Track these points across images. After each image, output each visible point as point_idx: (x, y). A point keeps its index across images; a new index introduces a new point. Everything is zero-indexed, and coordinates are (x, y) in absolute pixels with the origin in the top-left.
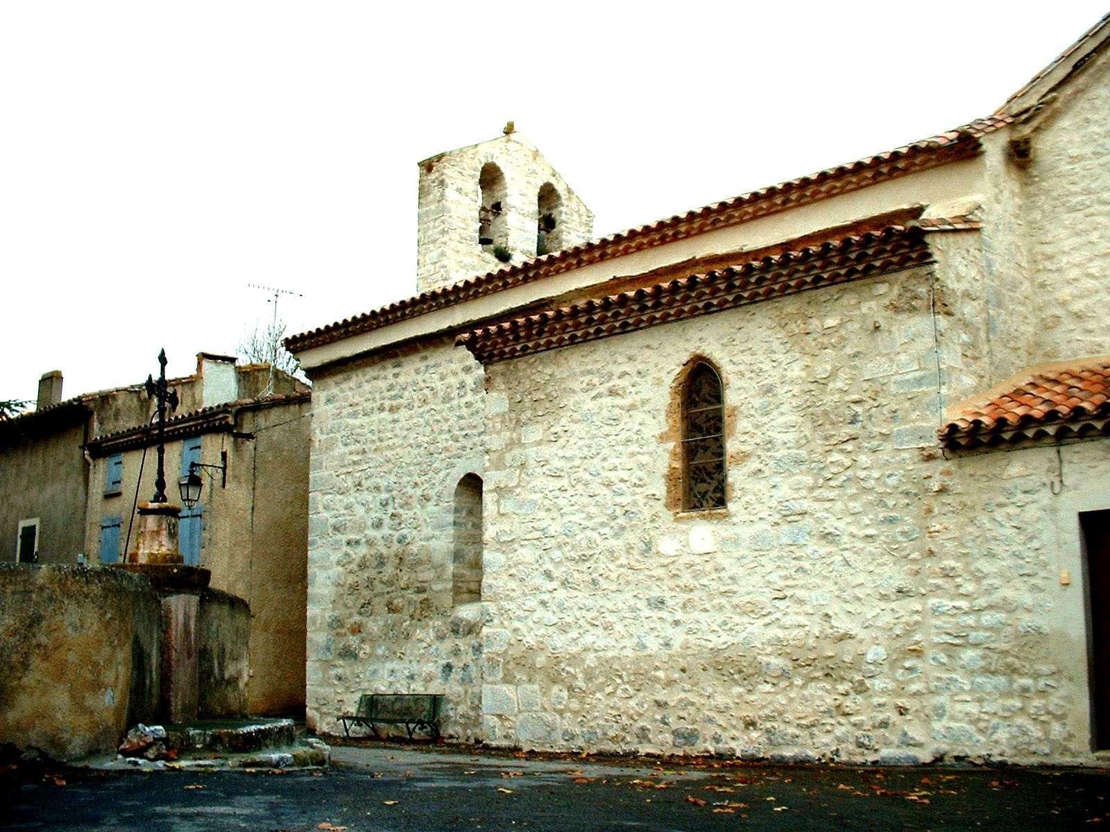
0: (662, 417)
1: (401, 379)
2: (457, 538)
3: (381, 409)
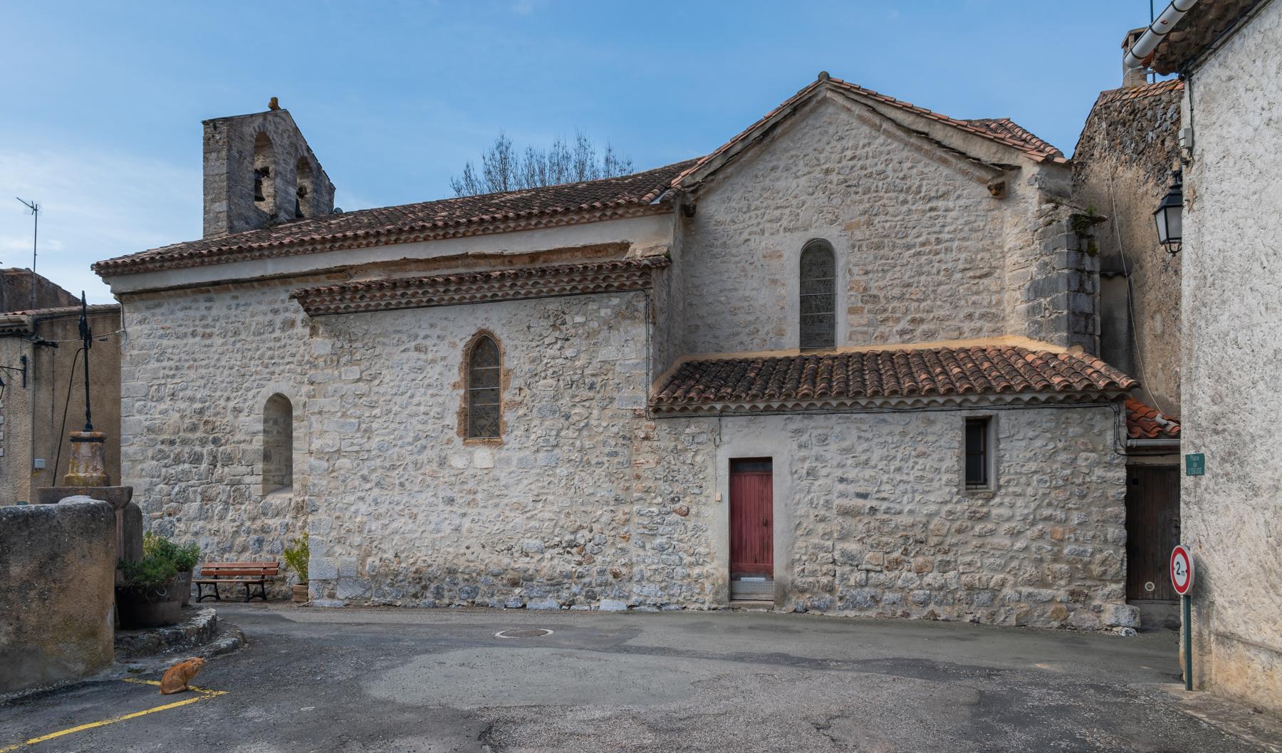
0: (456, 370)
1: (214, 312)
2: (266, 442)
3: (194, 334)
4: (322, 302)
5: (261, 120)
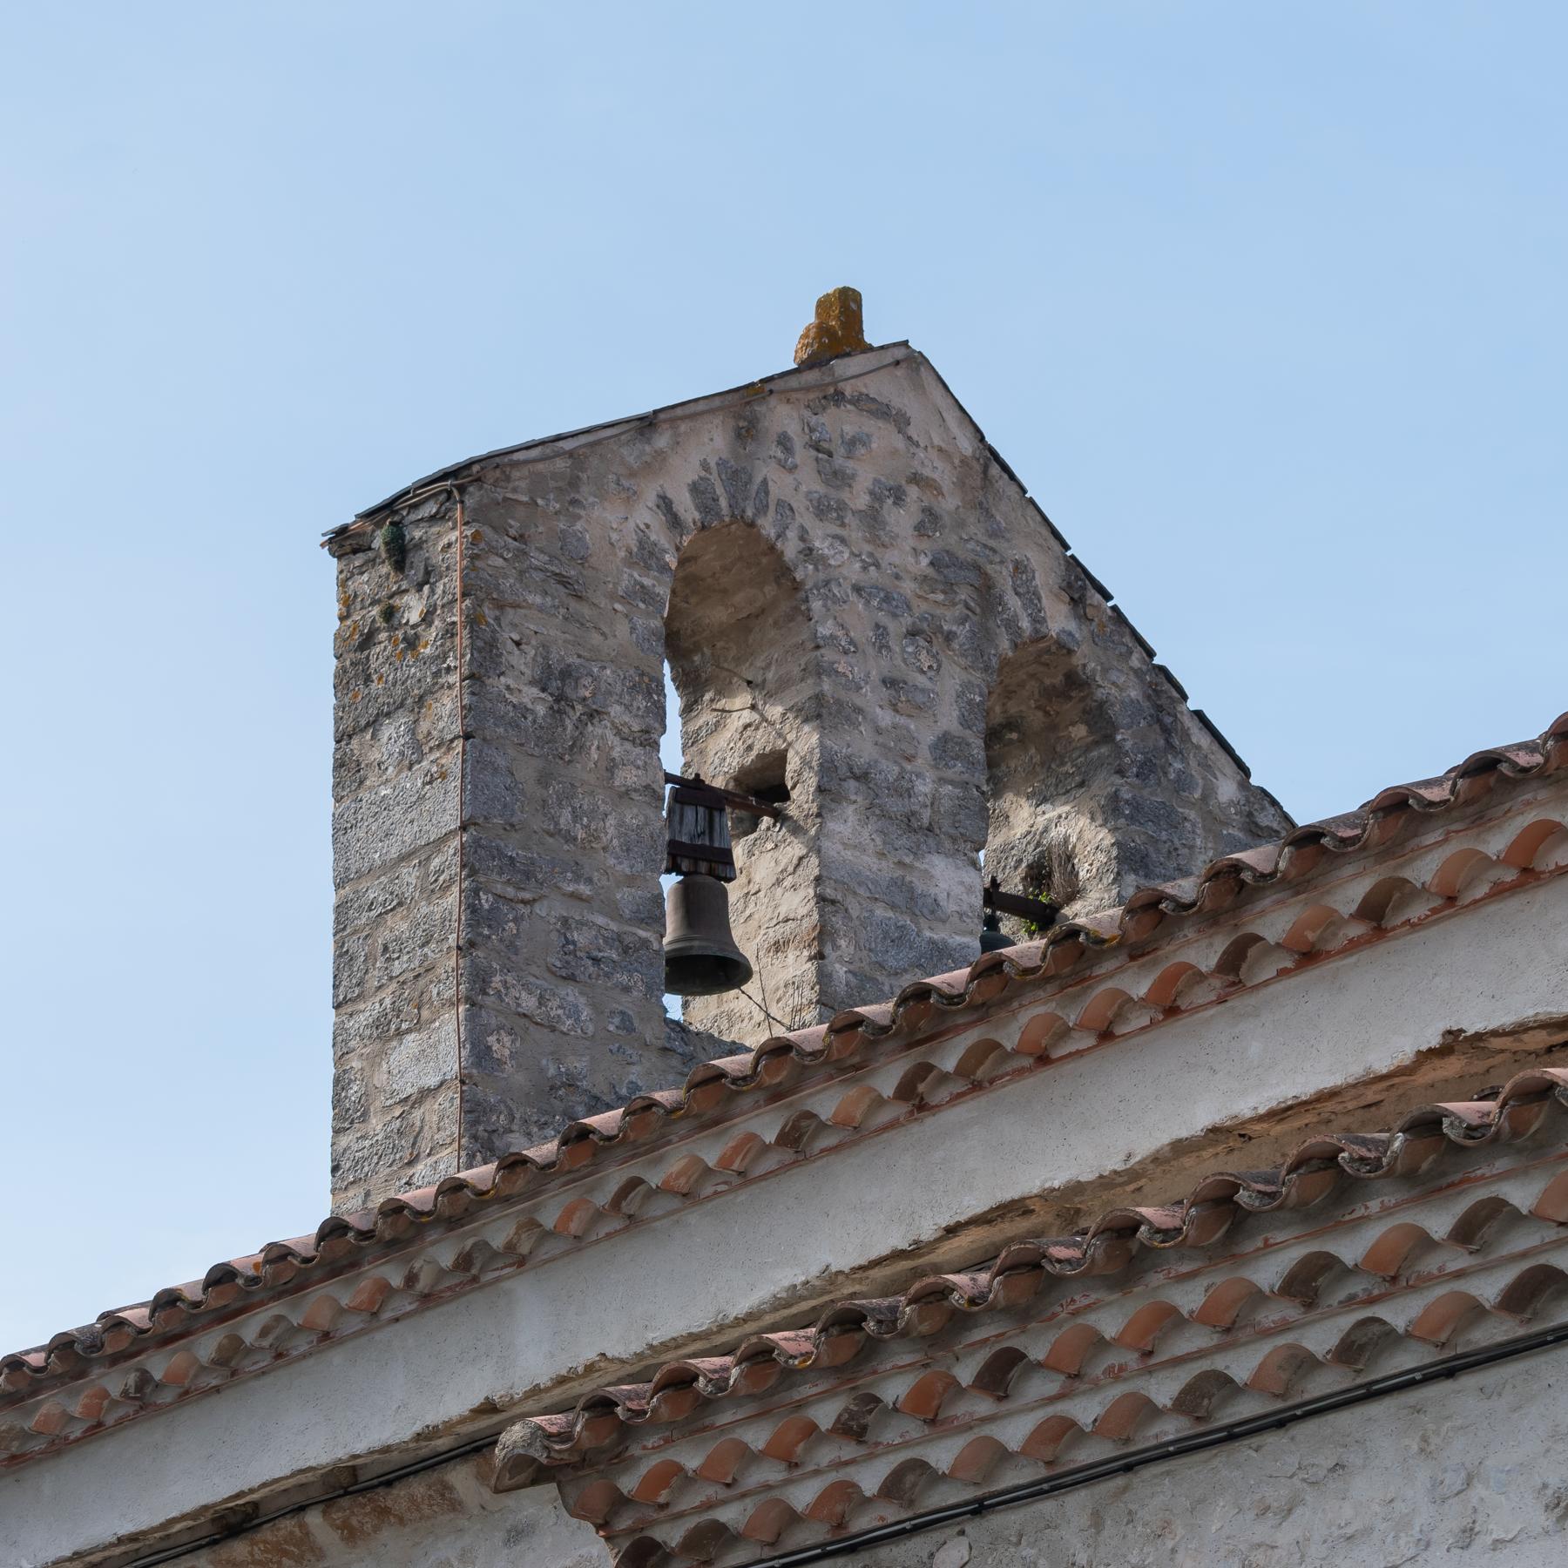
4: (728, 1472)
5: (714, 441)
